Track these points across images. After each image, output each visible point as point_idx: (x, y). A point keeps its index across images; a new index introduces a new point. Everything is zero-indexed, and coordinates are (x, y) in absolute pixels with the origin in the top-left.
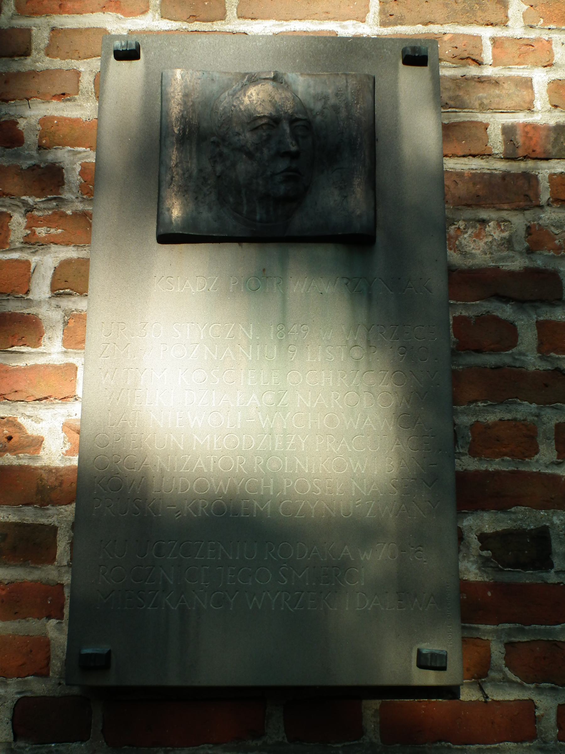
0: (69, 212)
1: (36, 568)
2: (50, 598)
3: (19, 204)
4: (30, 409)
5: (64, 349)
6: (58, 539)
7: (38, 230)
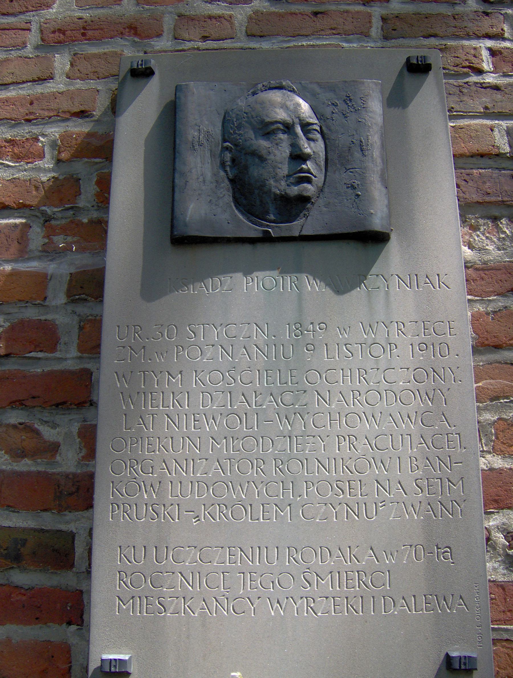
0: (85, 221)
1: (56, 573)
2: (69, 604)
3: (38, 214)
4: (47, 414)
5: (79, 354)
6: (76, 545)
7: (55, 238)
